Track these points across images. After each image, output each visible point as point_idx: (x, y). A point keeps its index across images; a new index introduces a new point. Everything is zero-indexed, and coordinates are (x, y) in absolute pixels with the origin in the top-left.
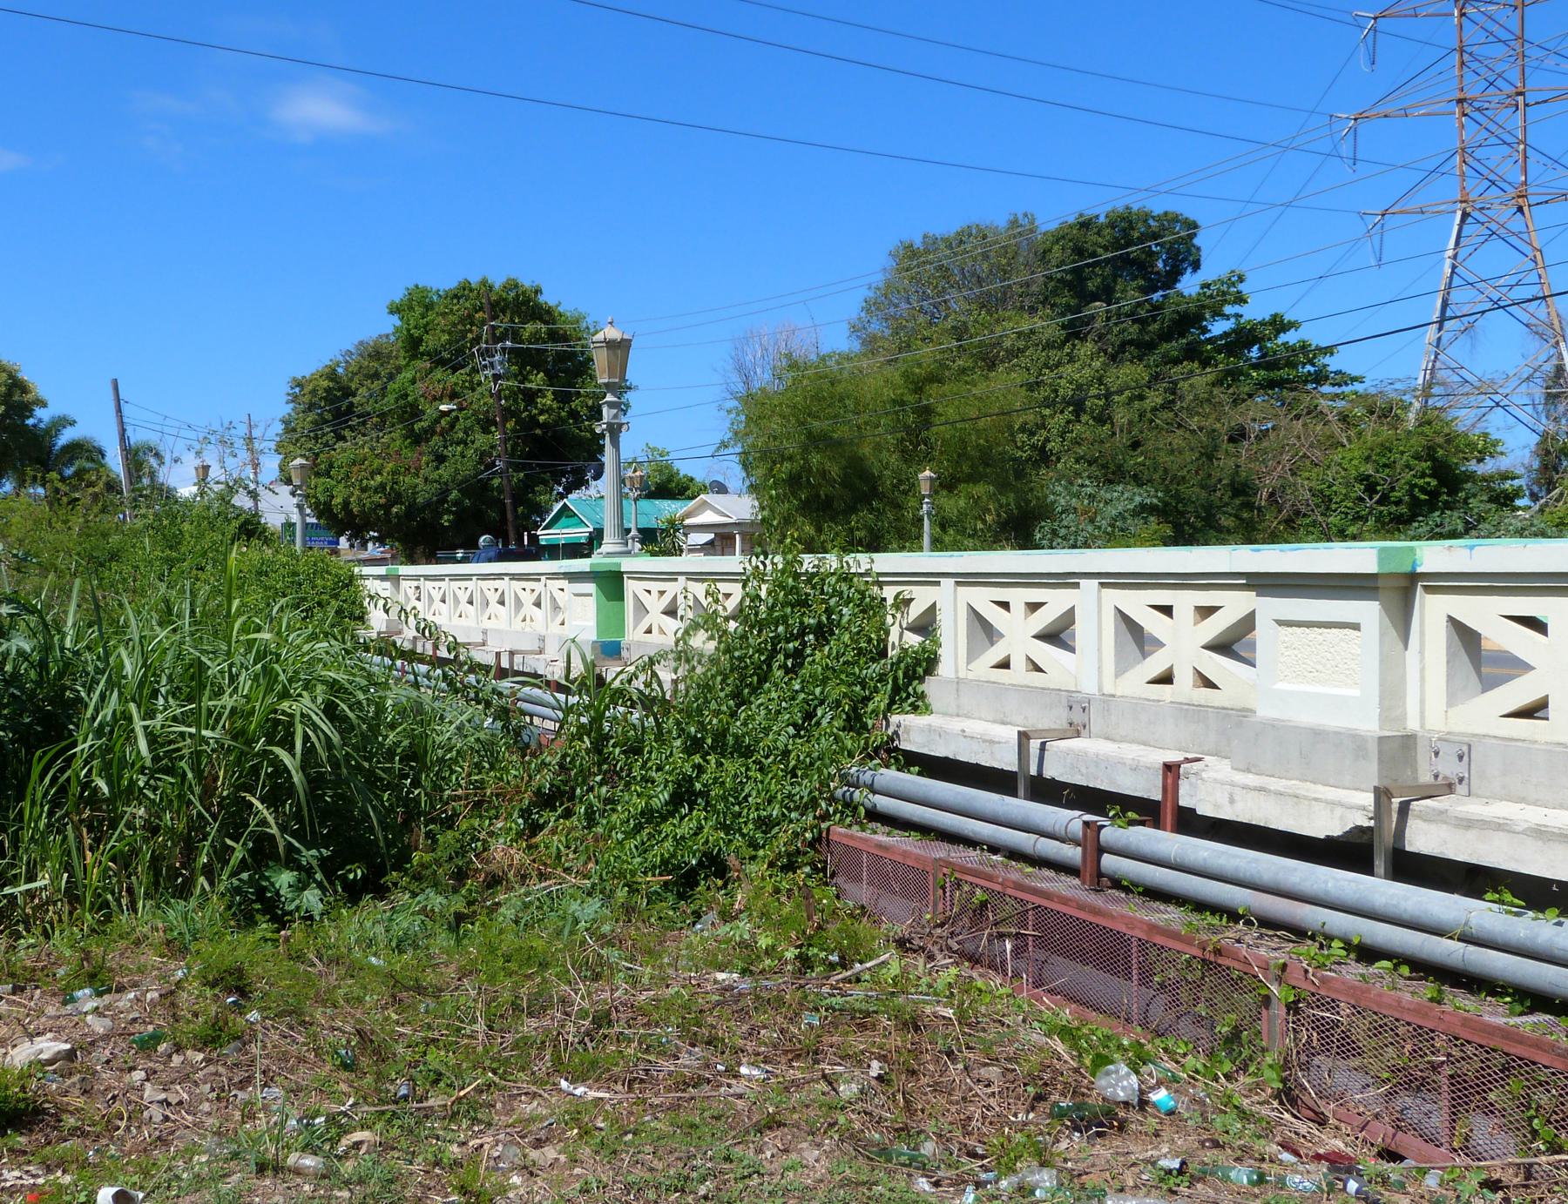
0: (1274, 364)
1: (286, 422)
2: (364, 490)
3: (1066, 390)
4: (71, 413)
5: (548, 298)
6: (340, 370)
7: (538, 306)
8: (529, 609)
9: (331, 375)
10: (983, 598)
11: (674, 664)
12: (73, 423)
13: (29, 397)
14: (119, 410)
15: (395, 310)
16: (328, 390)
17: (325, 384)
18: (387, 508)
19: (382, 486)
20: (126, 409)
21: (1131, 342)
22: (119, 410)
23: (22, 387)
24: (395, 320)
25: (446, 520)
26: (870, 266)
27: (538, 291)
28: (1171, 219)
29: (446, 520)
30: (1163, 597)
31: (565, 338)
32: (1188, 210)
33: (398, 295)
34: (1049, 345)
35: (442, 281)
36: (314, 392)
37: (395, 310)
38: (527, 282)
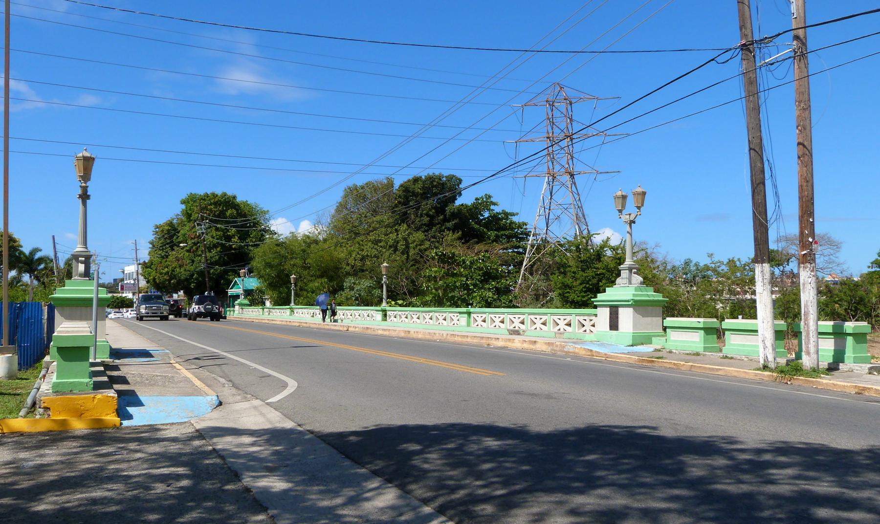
0: (503, 229)
1: (151, 243)
2: (161, 274)
3: (391, 242)
4: (41, 247)
5: (239, 199)
6: (175, 221)
7: (233, 203)
8: (441, 321)
9: (171, 224)
10: (512, 317)
11: (772, 365)
12: (40, 250)
13: (16, 244)
14: (55, 247)
15: (183, 202)
16: (168, 230)
17: (167, 228)
18: (169, 280)
19: (168, 272)
20: (57, 246)
21: (424, 225)
22: (55, 247)
23: (14, 241)
24: (183, 207)
25: (192, 286)
26: (337, 196)
27: (234, 197)
28: (451, 178)
29: (192, 286)
30: (586, 318)
31: (245, 216)
32: (458, 174)
33: (184, 196)
34: (387, 226)
35: (201, 191)
36: (162, 231)
37: (183, 202)
38: (230, 193)
